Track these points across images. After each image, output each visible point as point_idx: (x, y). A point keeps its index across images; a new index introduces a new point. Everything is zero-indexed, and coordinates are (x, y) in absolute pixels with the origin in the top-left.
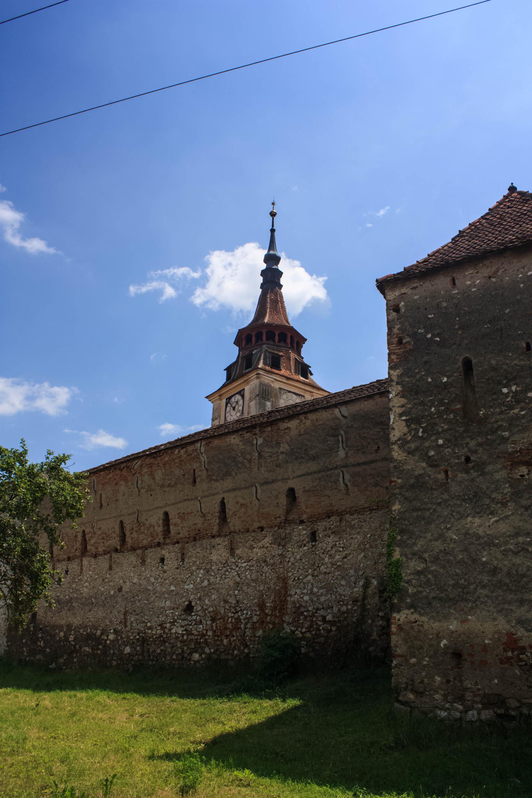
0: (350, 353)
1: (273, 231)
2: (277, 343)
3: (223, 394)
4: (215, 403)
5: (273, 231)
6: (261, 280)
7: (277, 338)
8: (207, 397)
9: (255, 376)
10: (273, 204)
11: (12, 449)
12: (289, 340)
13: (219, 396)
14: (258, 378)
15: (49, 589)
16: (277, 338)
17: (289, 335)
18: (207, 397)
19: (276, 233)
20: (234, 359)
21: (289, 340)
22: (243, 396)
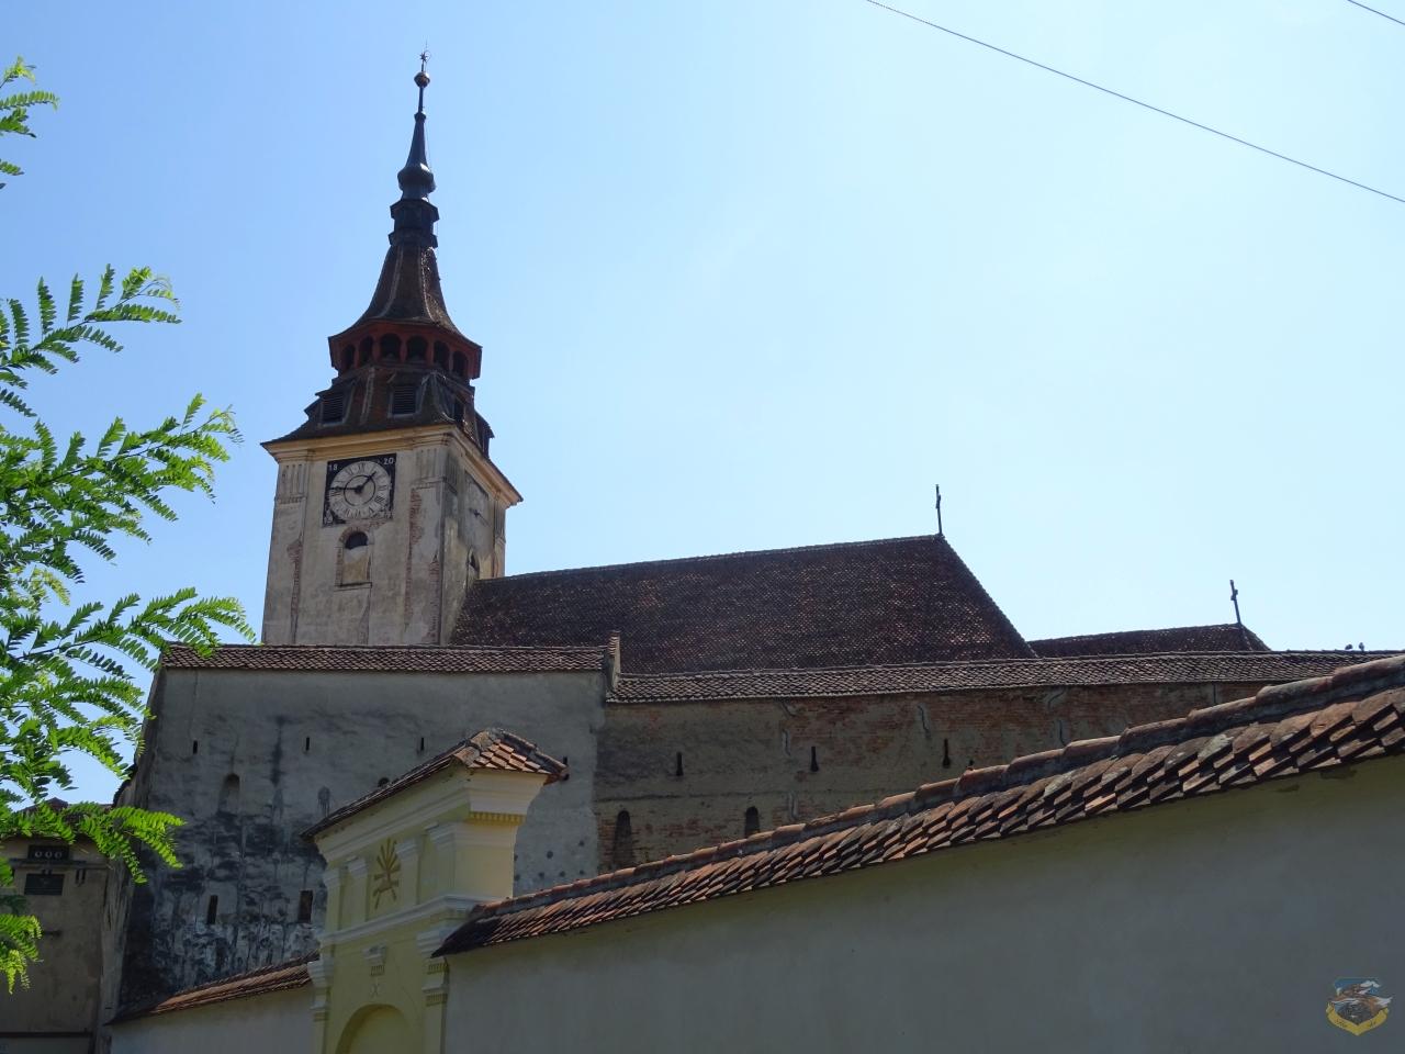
0: (472, 383)
1: (420, 118)
2: (450, 373)
3: (321, 450)
4: (285, 464)
5: (420, 118)
6: (389, 225)
7: (404, 348)
8: (265, 445)
9: (440, 437)
10: (423, 57)
11: (215, 634)
12: (431, 353)
13: (309, 450)
14: (446, 442)
15: (155, 835)
16: (404, 348)
17: (452, 350)
18: (265, 445)
19: (427, 125)
20: (1274, 648)
21: (431, 353)
22: (391, 470)
